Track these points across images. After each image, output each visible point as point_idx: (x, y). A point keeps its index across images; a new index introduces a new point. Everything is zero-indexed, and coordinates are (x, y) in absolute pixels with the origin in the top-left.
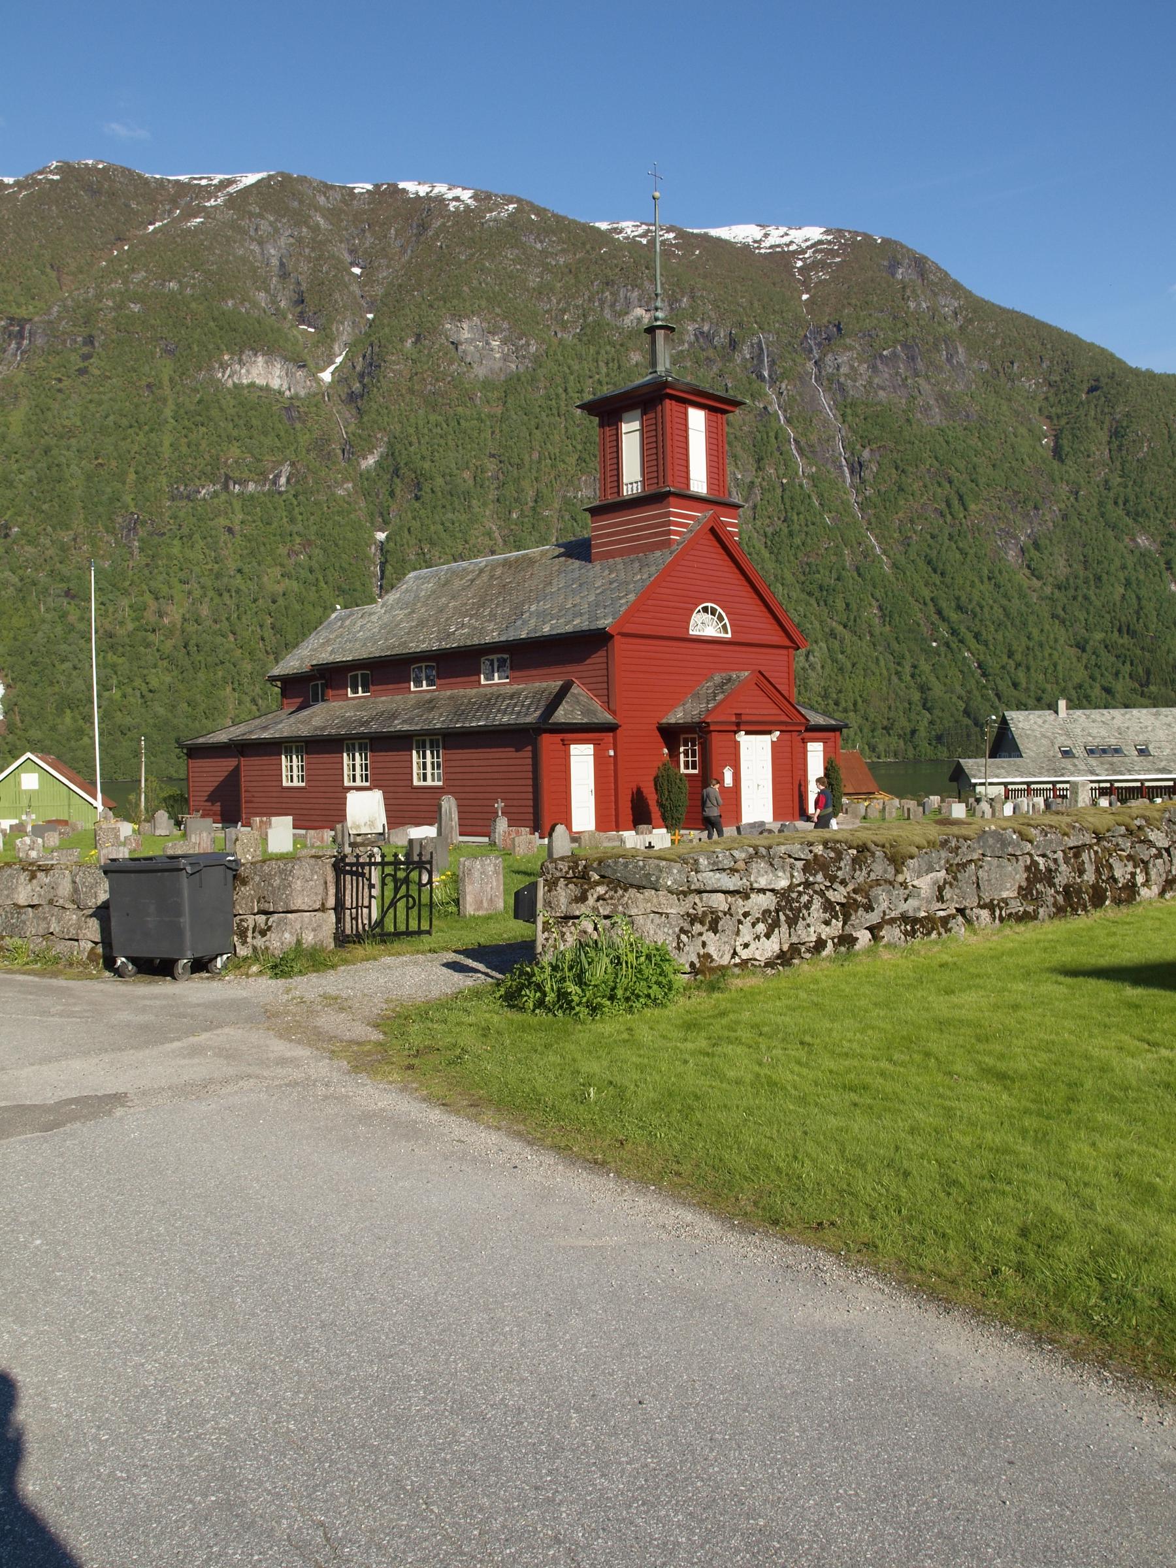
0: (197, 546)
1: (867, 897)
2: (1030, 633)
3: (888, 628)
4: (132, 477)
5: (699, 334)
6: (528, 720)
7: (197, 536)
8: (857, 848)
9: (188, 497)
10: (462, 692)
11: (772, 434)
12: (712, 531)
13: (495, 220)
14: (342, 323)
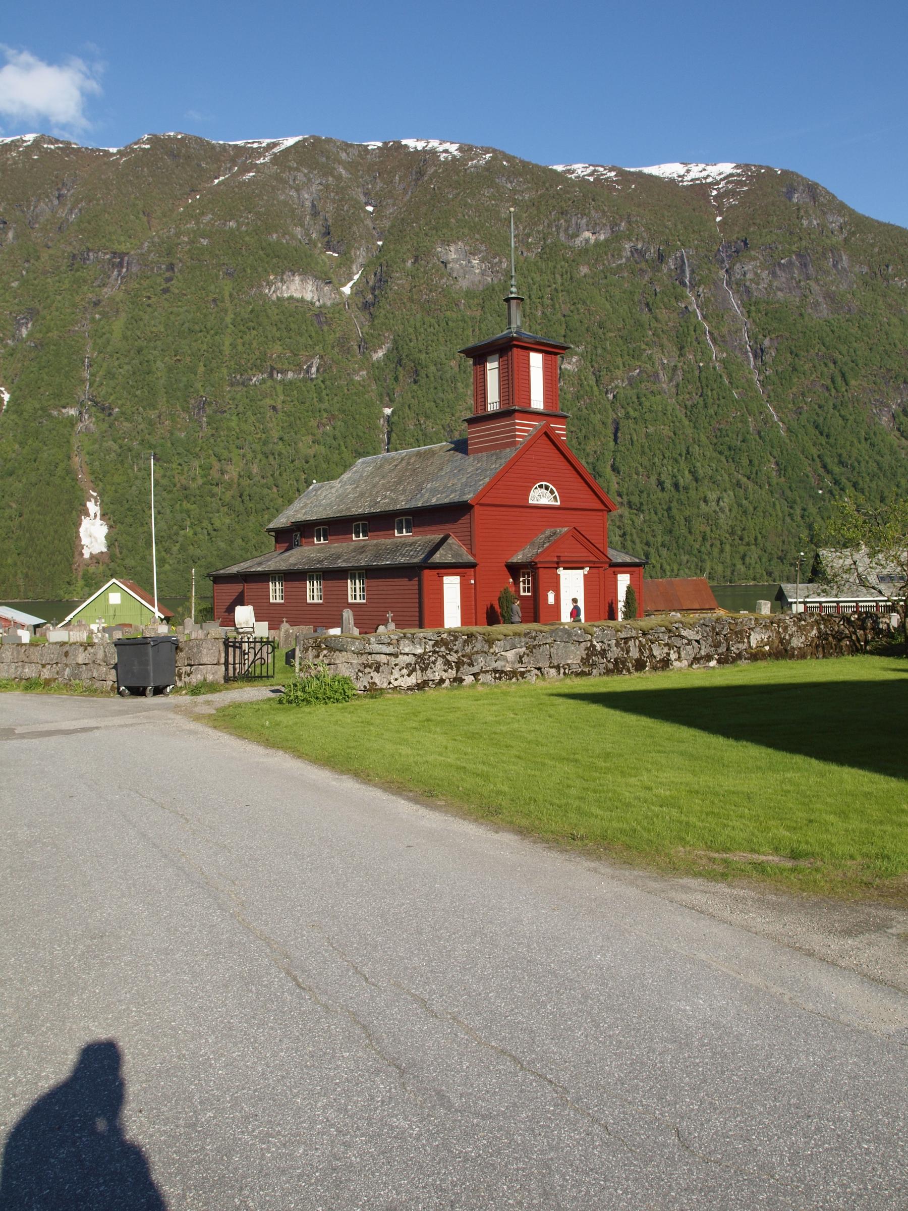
0: (250, 421)
1: (470, 659)
2: (899, 483)
3: (783, 479)
4: (201, 369)
5: (634, 251)
6: (416, 560)
7: (249, 413)
8: (467, 635)
9: (243, 384)
10: (382, 541)
11: (692, 328)
12: (546, 433)
13: (476, 167)
14: (359, 249)
